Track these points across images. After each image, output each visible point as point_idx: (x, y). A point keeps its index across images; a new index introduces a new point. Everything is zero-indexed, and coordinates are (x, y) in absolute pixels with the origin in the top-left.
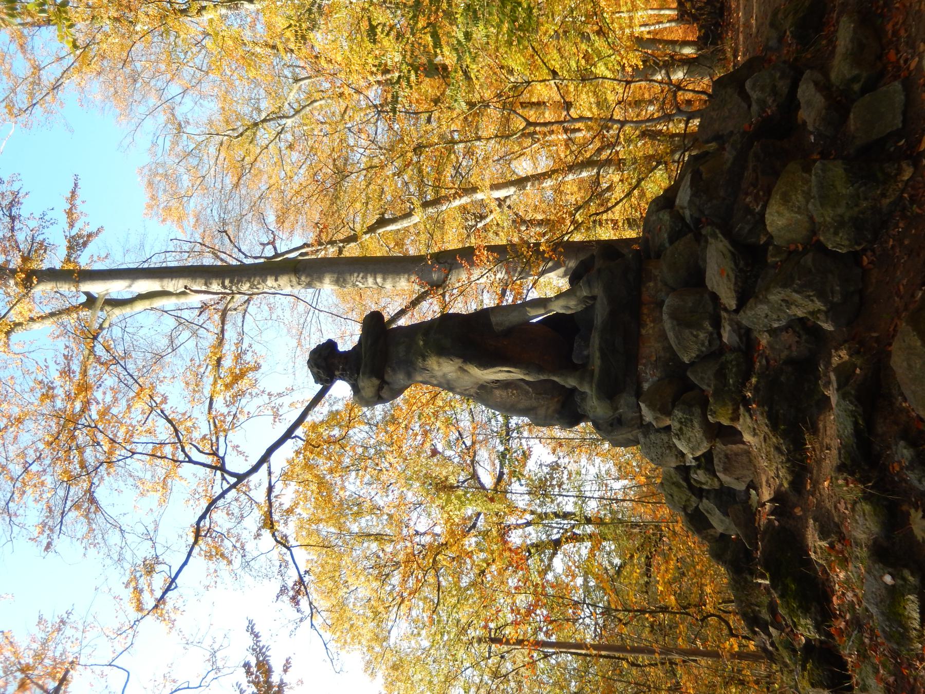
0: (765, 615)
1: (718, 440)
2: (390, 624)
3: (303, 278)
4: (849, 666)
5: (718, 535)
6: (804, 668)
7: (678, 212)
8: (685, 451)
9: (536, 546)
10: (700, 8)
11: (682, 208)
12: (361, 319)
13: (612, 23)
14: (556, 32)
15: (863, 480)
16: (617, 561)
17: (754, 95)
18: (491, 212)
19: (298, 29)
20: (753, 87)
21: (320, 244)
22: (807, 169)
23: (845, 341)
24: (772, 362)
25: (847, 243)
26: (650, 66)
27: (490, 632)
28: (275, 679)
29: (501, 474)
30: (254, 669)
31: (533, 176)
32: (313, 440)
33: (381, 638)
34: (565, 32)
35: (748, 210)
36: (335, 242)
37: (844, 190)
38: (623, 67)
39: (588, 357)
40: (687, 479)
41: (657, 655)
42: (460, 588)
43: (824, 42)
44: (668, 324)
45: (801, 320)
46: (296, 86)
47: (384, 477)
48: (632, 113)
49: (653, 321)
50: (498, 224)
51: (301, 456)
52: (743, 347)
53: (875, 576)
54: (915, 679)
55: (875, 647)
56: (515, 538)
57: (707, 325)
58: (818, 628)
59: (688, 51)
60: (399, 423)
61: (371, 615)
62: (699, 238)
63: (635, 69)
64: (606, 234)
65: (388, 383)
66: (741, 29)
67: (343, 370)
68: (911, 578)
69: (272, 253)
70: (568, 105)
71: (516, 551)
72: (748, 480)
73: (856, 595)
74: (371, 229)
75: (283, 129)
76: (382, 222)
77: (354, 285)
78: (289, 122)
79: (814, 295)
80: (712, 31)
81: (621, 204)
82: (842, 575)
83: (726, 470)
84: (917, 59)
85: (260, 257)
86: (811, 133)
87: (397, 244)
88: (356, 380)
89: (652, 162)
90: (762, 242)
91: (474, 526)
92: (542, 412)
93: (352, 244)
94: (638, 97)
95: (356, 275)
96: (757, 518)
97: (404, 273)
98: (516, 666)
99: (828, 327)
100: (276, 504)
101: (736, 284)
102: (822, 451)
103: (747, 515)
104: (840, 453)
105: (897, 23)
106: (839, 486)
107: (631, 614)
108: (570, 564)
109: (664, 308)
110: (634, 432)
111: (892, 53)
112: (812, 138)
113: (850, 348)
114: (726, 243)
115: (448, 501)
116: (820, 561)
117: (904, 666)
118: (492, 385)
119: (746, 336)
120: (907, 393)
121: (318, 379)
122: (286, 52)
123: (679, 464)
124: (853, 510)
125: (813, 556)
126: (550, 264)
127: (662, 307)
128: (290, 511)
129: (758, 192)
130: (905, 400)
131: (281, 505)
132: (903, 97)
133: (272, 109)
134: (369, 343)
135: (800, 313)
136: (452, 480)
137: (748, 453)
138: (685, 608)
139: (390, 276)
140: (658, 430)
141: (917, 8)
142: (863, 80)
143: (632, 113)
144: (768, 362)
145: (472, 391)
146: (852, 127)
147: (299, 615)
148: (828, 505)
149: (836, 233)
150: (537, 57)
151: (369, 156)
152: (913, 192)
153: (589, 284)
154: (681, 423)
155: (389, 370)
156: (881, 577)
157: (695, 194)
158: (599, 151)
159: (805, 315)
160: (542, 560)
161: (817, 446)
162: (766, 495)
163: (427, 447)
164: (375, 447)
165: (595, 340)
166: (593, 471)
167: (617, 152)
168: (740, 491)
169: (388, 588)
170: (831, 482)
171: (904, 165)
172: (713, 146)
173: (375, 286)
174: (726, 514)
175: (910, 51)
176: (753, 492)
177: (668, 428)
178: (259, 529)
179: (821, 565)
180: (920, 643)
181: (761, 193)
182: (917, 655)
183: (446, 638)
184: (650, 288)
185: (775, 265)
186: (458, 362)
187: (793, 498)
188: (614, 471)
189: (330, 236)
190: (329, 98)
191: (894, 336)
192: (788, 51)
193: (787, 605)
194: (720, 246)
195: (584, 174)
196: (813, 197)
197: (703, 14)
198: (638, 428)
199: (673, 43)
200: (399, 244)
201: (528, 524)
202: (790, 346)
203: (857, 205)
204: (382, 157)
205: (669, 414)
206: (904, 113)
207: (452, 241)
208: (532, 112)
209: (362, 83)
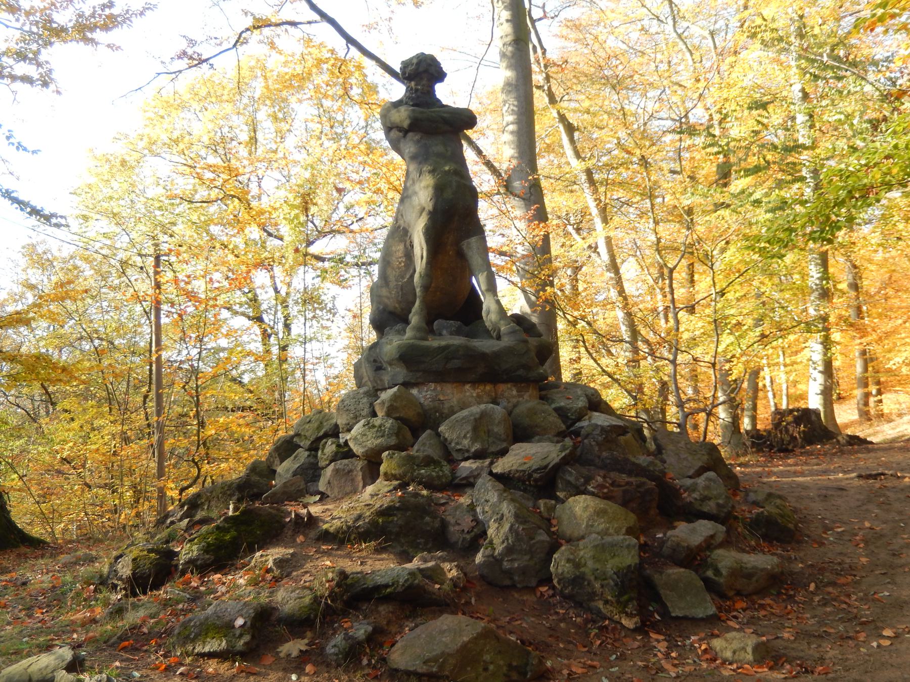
0: (199, 515)
1: (366, 462)
2: (168, 156)
3: (510, 48)
4: (155, 592)
5: (274, 468)
6: (150, 551)
7: (586, 414)
8: (352, 432)
9: (255, 299)
10: (787, 431)
11: (590, 418)
12: (470, 108)
13: (772, 348)
14: (763, 293)
15: (332, 595)
16: (246, 379)
17: (701, 481)
18: (584, 239)
19: (763, 28)
20: (710, 480)
21: (546, 66)
22: (630, 531)
23: (465, 574)
24: (443, 508)
25: (560, 571)
26: (733, 388)
27: (165, 255)
28: (98, 35)
29: (322, 260)
30: (107, 11)
31: (620, 278)
32: (346, 66)
33: (152, 148)
34: (764, 303)
35: (588, 480)
36: (548, 81)
37: (611, 566)
38: (729, 361)
39: (440, 335)
40: (326, 435)
41: (156, 418)
42: (208, 225)
43: (753, 543)
44: (476, 409)
45: (484, 533)
46: (706, 33)
47: (313, 142)
48: (684, 371)
49: (478, 396)
50: (571, 246)
51: (329, 55)
52: (456, 481)
53: (242, 610)
54: (146, 651)
55: (175, 614)
56: (261, 278)
57: (477, 446)
58: (191, 562)
59: (746, 424)
60: (368, 155)
61: (175, 137)
62: (562, 435)
63: (728, 373)
64: (565, 353)
65: (405, 136)
66: (766, 469)
67: (417, 90)
68: (242, 642)
69: (535, 17)
70: (691, 310)
71: (248, 278)
72: (329, 493)
73: (223, 594)
74: (562, 118)
75: (662, 21)
76: (570, 129)
77: (505, 102)
78: (669, 27)
79: (508, 544)
80: (765, 442)
81: (595, 365)
82: (242, 581)
83: (336, 471)
84: (737, 627)
85: (530, 4)
86: (665, 534)
87: (549, 146)
88: (406, 103)
89: (636, 393)
90: (558, 493)
91: (270, 235)
92: (384, 292)
93: (547, 100)
94: (700, 377)
95: (516, 103)
96: (293, 503)
97: (519, 153)
98: (134, 283)
99: (479, 558)
100: (279, 30)
101: (517, 471)
102: (359, 558)
103: (295, 495)
104: (358, 573)
105: (772, 608)
106: (326, 575)
107: (193, 392)
108: (239, 332)
109: (492, 405)
110: (369, 383)
111: (744, 605)
112: (660, 535)
113: (459, 578)
114: (557, 460)
115: (293, 207)
116: (254, 560)
117: (159, 640)
118: (408, 242)
119: (467, 484)
120: (418, 631)
121: (405, 65)
122: (740, 21)
123: (340, 426)
124: (304, 588)
125: (258, 554)
126: (533, 298)
127: (492, 403)
128: (272, 45)
129: (607, 487)
130: (411, 630)
131: (279, 35)
132: (701, 616)
133: (683, 9)
134: (445, 115)
135: (491, 532)
136: (313, 210)
137: (355, 491)
138: (204, 444)
139: (516, 139)
140: (372, 405)
141: (786, 625)
142: (716, 579)
143: (684, 371)
144: (443, 504)
145: (401, 222)
146: (670, 571)
147: (168, 60)
148: (308, 566)
149: (568, 561)
150: (737, 275)
151: (636, 113)
152: (610, 628)
153: (513, 332)
154: (380, 427)
155: (417, 137)
156: (242, 616)
157: (603, 429)
158: (647, 342)
159: (489, 535)
160: (241, 305)
161: (364, 553)
162: (315, 510)
163: (347, 185)
164: (345, 133)
165: (457, 341)
166: (332, 351)
167: (645, 358)
168: (317, 486)
169: (203, 153)
170: (330, 568)
171: (637, 619)
172: (652, 447)
173: (505, 124)
174: (295, 474)
175: (745, 621)
176: (318, 497)
177: (374, 414)
178: (252, 14)
179: (250, 562)
180: (182, 654)
181: (605, 490)
182: (170, 652)
183: (158, 213)
184: (509, 391)
185: (536, 506)
186: (429, 206)
187: (313, 534)
188: (334, 372)
189: (554, 76)
190: (695, 69)
191: (472, 617)
192: (744, 511)
193: (209, 533)
194: (554, 455)
195: (623, 328)
196: (602, 539)
197: (781, 433)
198: (374, 387)
199: (754, 408)
200: (549, 148)
201: (276, 291)
202: (459, 524)
203: (596, 578)
204: (635, 126)
205: (389, 414)
206: (685, 618)
207: (553, 201)
208: (684, 275)
209: (709, 101)
